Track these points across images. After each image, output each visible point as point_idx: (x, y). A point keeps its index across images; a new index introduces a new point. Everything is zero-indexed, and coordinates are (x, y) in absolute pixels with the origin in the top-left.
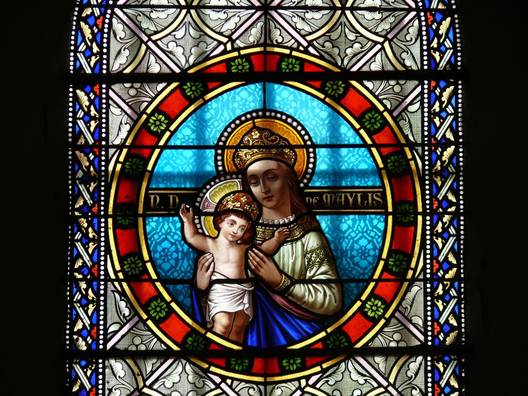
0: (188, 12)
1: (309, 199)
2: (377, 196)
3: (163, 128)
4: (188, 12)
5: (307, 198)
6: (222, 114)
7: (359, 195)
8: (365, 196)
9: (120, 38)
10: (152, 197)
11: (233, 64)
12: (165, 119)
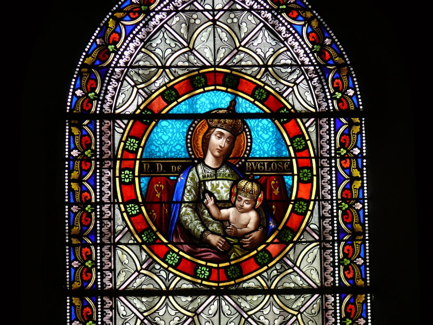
0: (164, 70)
1: (174, 168)
2: (280, 164)
3: (304, 143)
4: (164, 70)
5: (172, 167)
6: (218, 100)
7: (266, 163)
8: (269, 164)
9: (122, 315)
10: (145, 165)
11: (305, 204)
12: (300, 138)
